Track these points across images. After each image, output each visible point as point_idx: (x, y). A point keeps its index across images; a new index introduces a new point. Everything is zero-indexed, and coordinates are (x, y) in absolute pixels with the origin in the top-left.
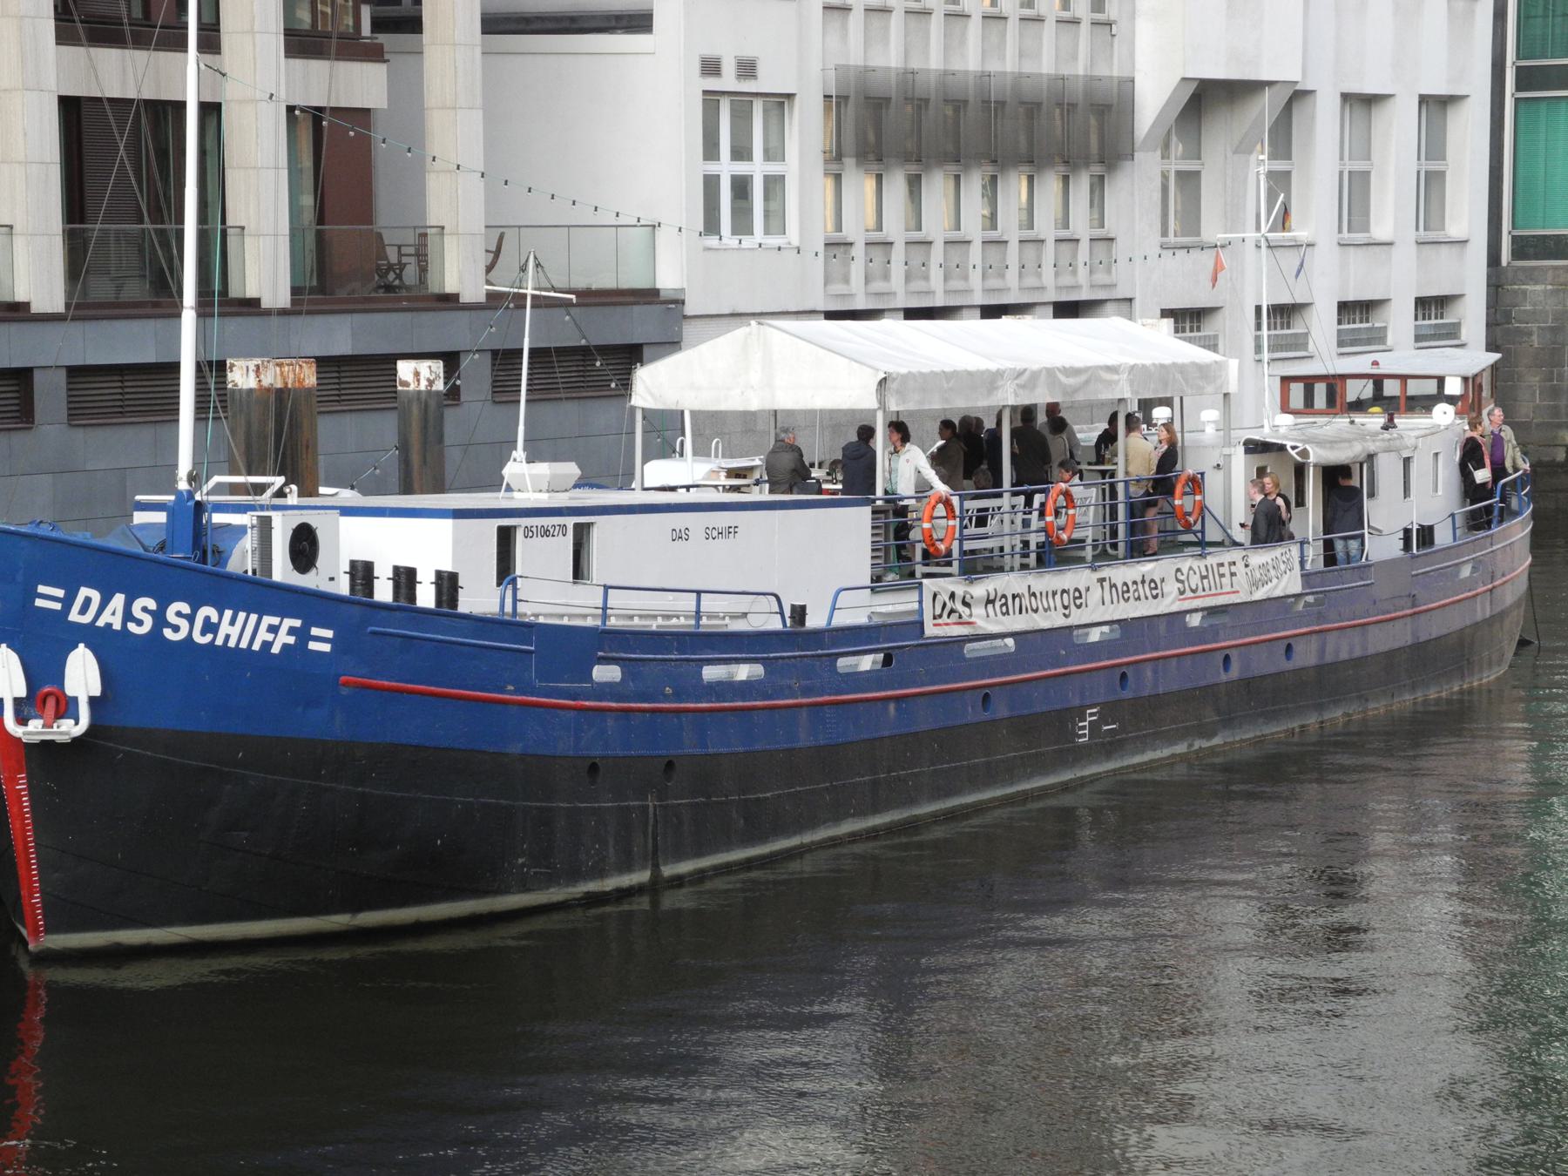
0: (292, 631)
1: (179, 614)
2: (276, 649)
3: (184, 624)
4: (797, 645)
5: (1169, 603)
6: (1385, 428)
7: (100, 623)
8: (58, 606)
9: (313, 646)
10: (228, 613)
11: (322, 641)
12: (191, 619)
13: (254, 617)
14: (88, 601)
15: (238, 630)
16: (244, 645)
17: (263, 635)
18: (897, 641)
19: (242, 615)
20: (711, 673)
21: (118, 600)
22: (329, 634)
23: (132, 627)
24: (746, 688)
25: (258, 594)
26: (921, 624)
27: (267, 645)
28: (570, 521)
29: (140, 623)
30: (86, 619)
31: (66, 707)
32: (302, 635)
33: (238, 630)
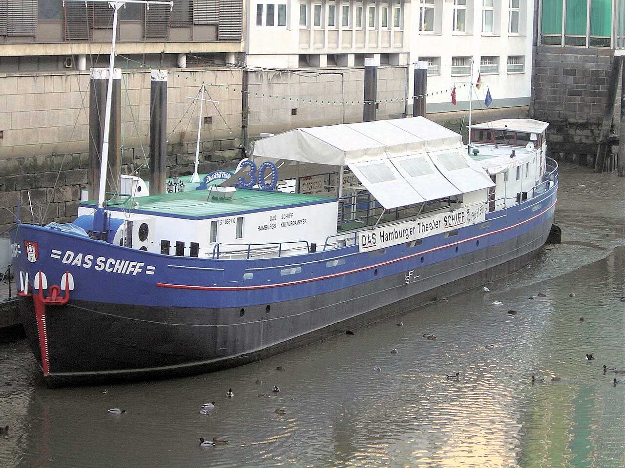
0: (140, 267)
1: (101, 261)
2: (134, 274)
3: (103, 265)
7: (73, 264)
8: (59, 257)
9: (148, 272)
10: (118, 261)
11: (151, 271)
12: (105, 263)
13: (127, 262)
14: (70, 255)
16: (123, 272)
17: (130, 269)
18: (349, 254)
19: (123, 262)
20: (283, 272)
21: (80, 256)
22: (153, 268)
23: (84, 265)
24: (295, 277)
25: (125, 253)
27: (132, 272)
28: (236, 217)
29: (87, 264)
30: (69, 262)
32: (144, 269)
33: (122, 267)
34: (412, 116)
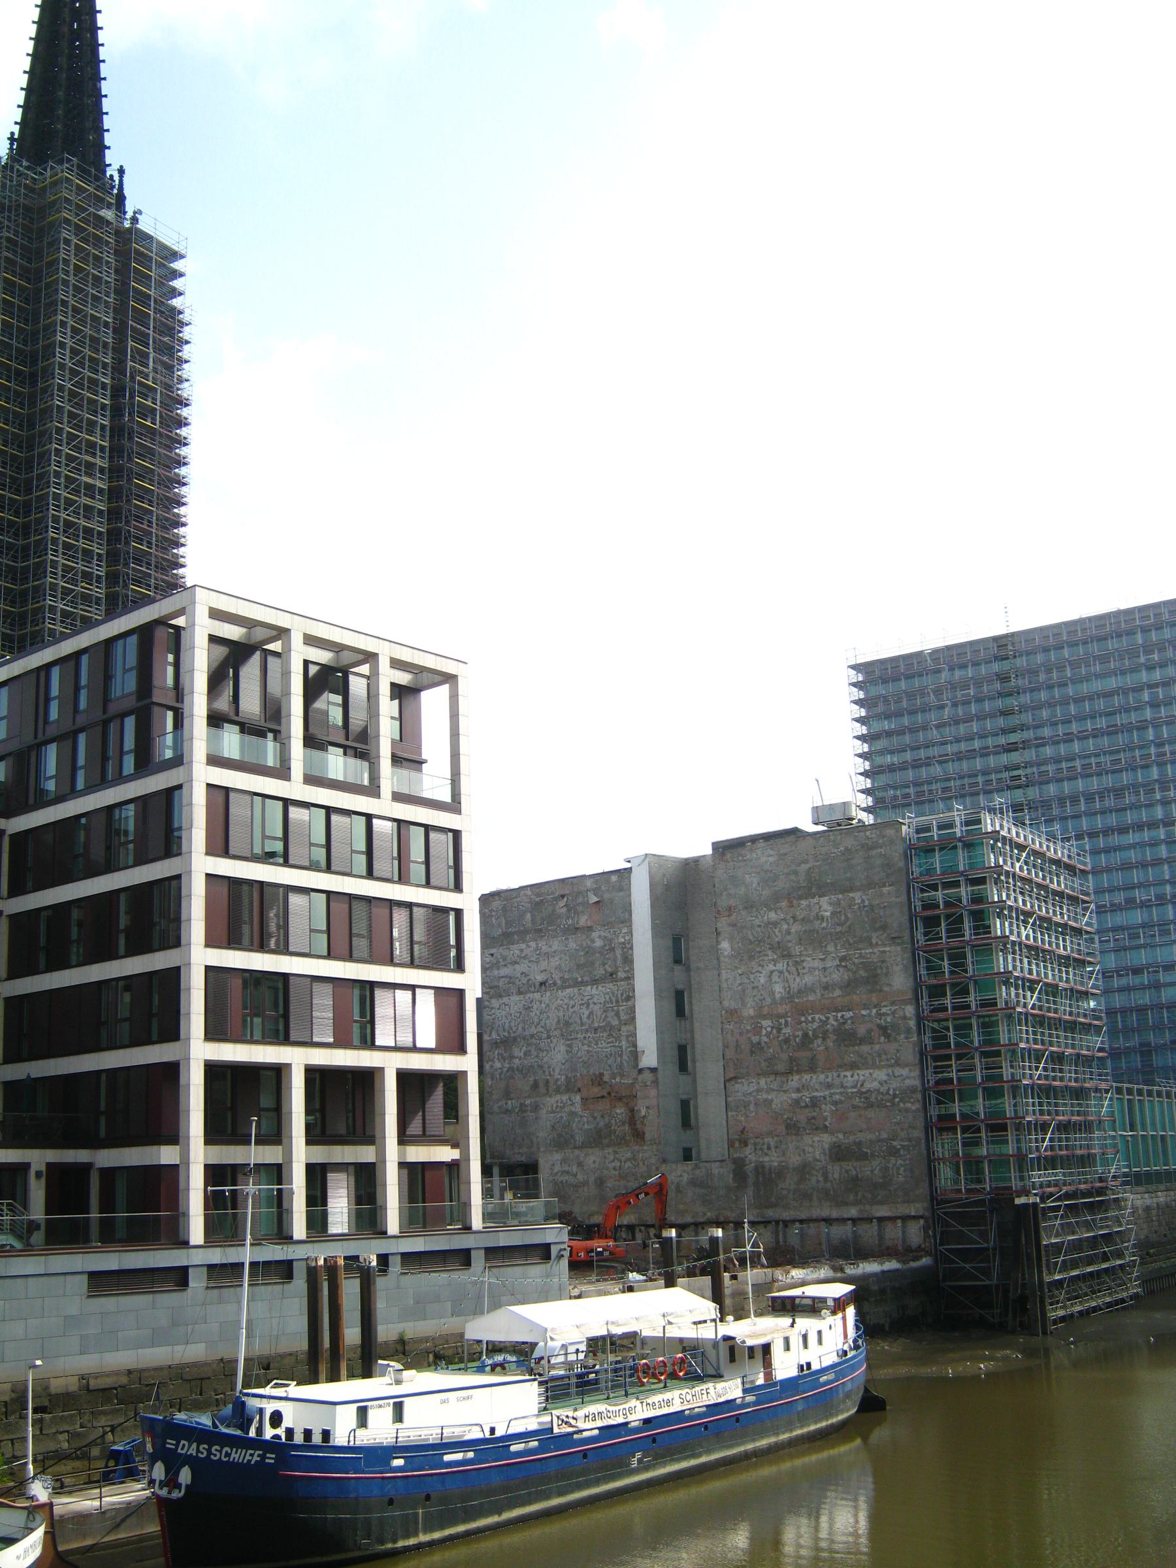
4: (492, 1446)
5: (676, 1407)
6: (792, 1326)
11: (271, 1459)
12: (220, 1452)
15: (237, 1455)
17: (248, 1457)
18: (545, 1435)
21: (194, 1445)
26: (552, 1429)
27: (249, 1461)
28: (392, 1401)
31: (179, 1486)
32: (263, 1457)
33: (237, 1455)
34: (38, 1237)
